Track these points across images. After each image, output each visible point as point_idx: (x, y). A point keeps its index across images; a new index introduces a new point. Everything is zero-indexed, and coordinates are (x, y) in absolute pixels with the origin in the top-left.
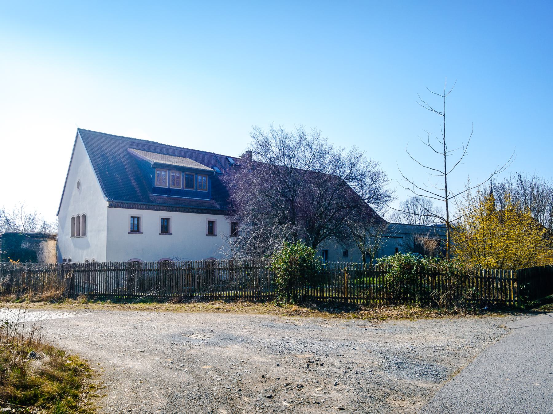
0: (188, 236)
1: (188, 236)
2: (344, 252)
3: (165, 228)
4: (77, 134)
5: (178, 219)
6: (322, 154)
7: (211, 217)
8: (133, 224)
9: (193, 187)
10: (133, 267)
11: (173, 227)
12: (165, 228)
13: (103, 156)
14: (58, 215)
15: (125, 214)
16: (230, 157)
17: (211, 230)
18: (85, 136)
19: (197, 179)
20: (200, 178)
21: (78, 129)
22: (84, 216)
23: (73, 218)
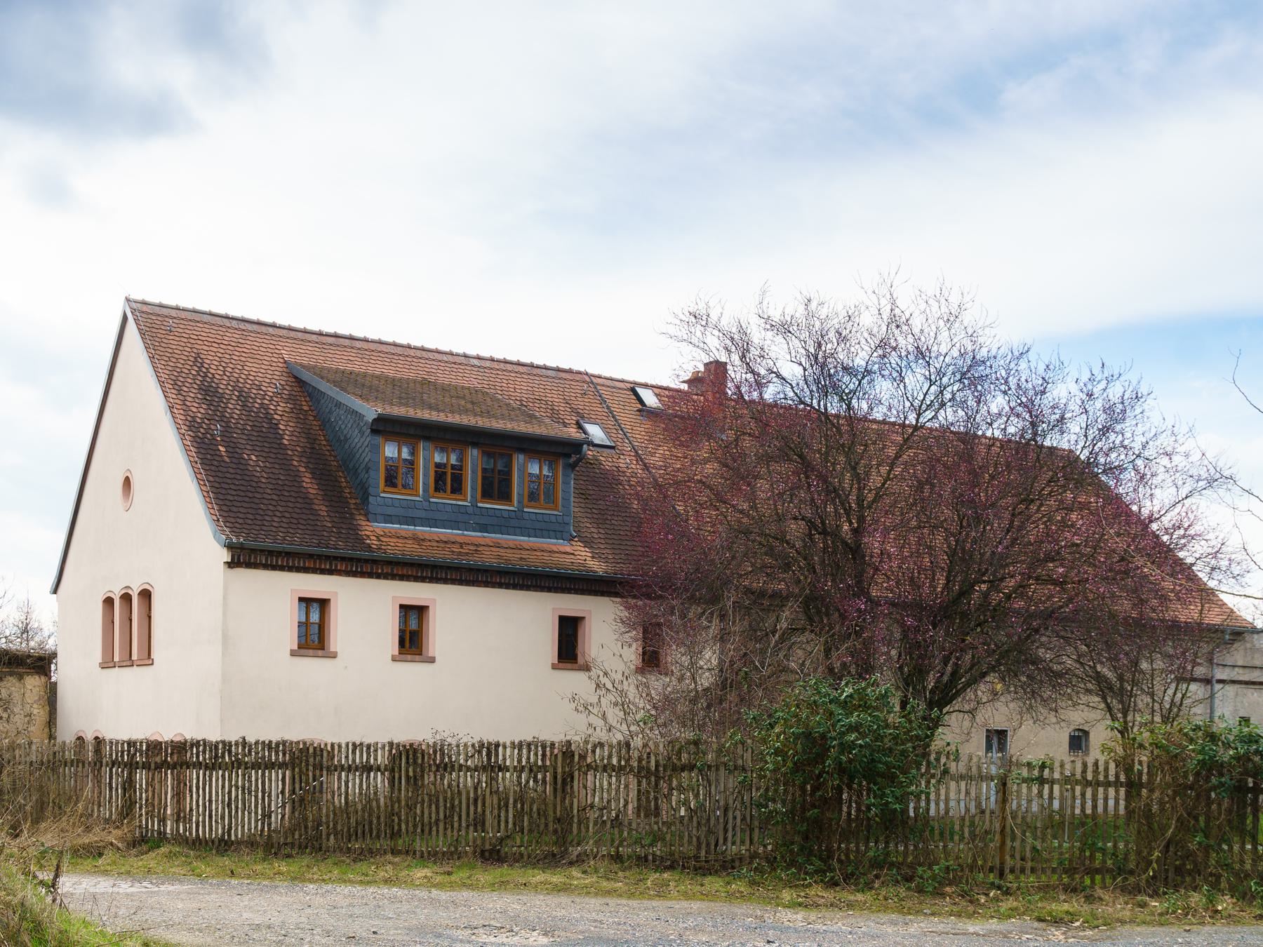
0: (489, 674)
1: (489, 674)
2: (1072, 738)
3: (412, 639)
4: (125, 319)
5: (454, 611)
6: (973, 374)
7: (572, 604)
8: (304, 626)
9: (505, 496)
10: (306, 762)
11: (439, 633)
12: (412, 639)
13: (209, 392)
14: (55, 591)
15: (279, 592)
16: (645, 386)
17: (314, 636)
18: (176, 341)
19: (523, 470)
20: (534, 469)
21: (128, 300)
22: (146, 595)
23: (109, 602)
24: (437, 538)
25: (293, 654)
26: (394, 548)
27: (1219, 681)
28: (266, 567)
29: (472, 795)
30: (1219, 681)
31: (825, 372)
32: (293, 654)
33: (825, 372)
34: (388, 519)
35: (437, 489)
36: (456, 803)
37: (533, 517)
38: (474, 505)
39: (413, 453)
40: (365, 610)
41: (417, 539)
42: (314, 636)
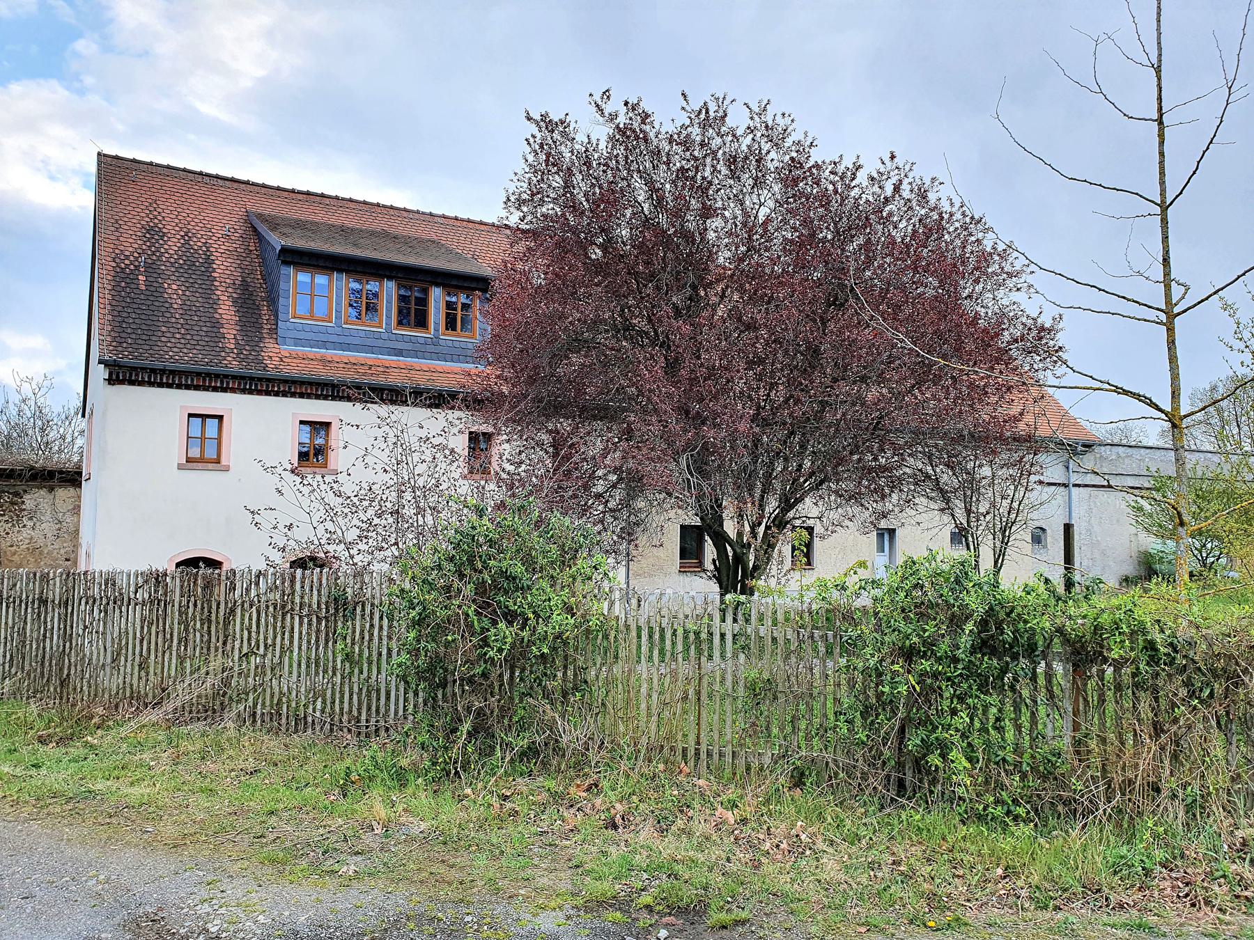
5: (357, 429)
17: (204, 454)
24: (340, 362)
25: (180, 467)
26: (293, 370)
27: (1075, 485)
28: (151, 384)
29: (138, 635)
30: (1075, 485)
31: (111, 21)
32: (180, 467)
33: (111, 21)
34: (298, 342)
35: (400, 323)
36: (124, 642)
37: (450, 344)
38: (388, 331)
39: (330, 281)
40: (262, 428)
41: (324, 361)
42: (204, 454)
